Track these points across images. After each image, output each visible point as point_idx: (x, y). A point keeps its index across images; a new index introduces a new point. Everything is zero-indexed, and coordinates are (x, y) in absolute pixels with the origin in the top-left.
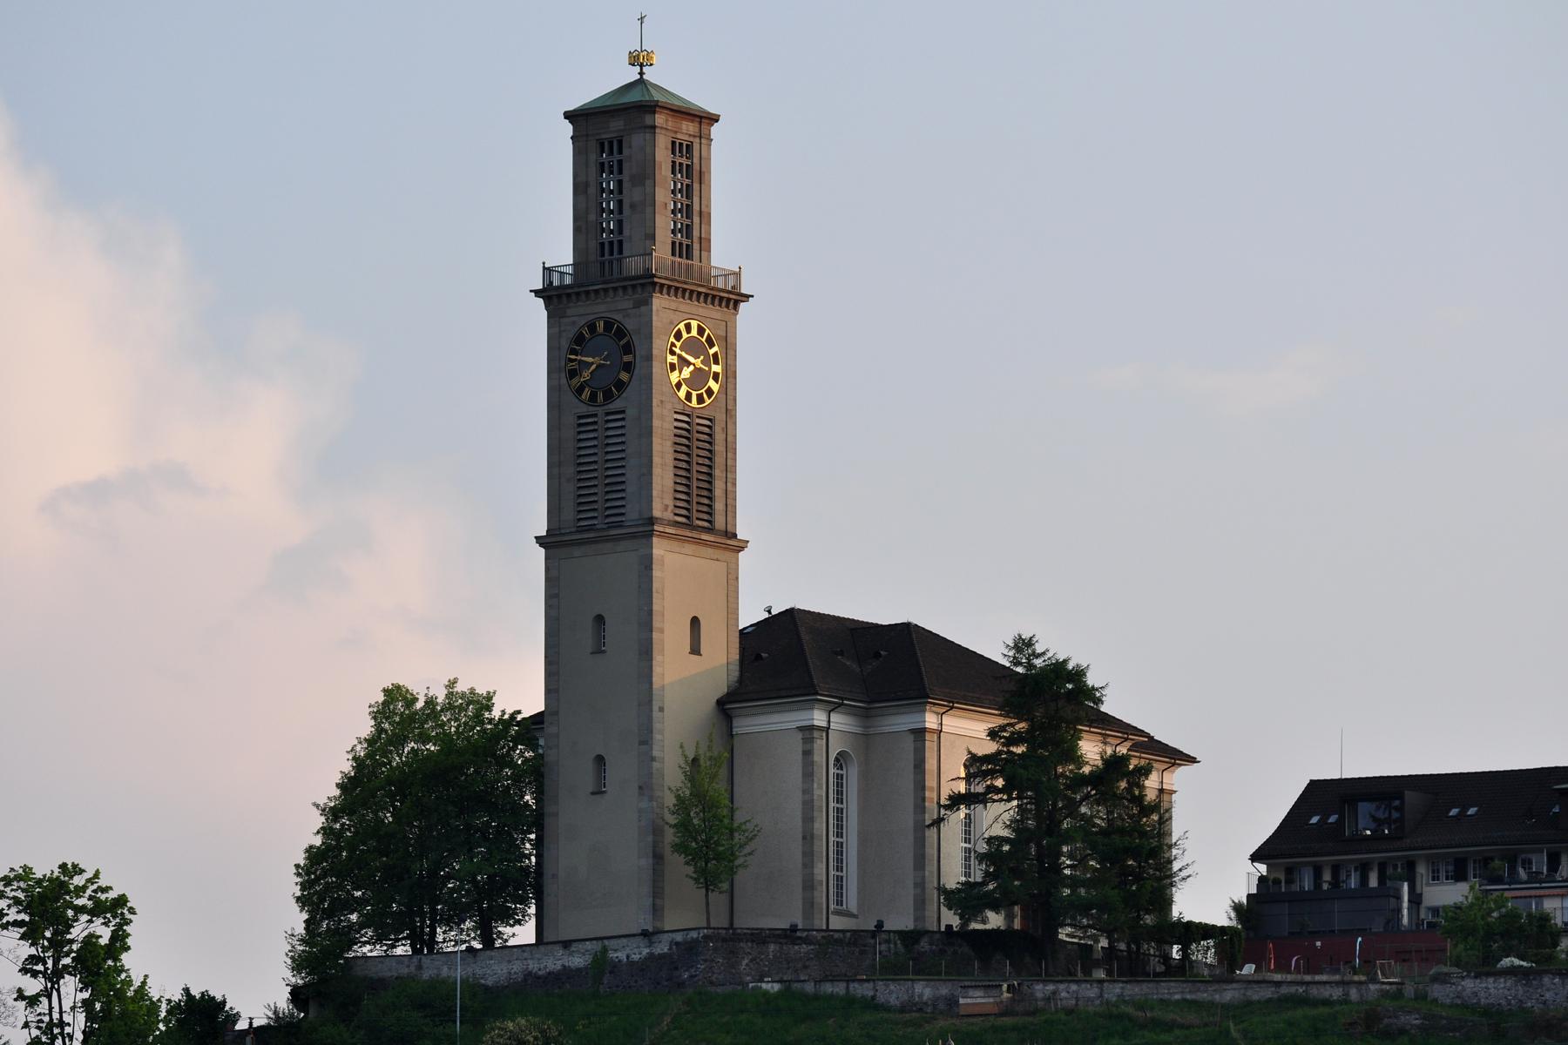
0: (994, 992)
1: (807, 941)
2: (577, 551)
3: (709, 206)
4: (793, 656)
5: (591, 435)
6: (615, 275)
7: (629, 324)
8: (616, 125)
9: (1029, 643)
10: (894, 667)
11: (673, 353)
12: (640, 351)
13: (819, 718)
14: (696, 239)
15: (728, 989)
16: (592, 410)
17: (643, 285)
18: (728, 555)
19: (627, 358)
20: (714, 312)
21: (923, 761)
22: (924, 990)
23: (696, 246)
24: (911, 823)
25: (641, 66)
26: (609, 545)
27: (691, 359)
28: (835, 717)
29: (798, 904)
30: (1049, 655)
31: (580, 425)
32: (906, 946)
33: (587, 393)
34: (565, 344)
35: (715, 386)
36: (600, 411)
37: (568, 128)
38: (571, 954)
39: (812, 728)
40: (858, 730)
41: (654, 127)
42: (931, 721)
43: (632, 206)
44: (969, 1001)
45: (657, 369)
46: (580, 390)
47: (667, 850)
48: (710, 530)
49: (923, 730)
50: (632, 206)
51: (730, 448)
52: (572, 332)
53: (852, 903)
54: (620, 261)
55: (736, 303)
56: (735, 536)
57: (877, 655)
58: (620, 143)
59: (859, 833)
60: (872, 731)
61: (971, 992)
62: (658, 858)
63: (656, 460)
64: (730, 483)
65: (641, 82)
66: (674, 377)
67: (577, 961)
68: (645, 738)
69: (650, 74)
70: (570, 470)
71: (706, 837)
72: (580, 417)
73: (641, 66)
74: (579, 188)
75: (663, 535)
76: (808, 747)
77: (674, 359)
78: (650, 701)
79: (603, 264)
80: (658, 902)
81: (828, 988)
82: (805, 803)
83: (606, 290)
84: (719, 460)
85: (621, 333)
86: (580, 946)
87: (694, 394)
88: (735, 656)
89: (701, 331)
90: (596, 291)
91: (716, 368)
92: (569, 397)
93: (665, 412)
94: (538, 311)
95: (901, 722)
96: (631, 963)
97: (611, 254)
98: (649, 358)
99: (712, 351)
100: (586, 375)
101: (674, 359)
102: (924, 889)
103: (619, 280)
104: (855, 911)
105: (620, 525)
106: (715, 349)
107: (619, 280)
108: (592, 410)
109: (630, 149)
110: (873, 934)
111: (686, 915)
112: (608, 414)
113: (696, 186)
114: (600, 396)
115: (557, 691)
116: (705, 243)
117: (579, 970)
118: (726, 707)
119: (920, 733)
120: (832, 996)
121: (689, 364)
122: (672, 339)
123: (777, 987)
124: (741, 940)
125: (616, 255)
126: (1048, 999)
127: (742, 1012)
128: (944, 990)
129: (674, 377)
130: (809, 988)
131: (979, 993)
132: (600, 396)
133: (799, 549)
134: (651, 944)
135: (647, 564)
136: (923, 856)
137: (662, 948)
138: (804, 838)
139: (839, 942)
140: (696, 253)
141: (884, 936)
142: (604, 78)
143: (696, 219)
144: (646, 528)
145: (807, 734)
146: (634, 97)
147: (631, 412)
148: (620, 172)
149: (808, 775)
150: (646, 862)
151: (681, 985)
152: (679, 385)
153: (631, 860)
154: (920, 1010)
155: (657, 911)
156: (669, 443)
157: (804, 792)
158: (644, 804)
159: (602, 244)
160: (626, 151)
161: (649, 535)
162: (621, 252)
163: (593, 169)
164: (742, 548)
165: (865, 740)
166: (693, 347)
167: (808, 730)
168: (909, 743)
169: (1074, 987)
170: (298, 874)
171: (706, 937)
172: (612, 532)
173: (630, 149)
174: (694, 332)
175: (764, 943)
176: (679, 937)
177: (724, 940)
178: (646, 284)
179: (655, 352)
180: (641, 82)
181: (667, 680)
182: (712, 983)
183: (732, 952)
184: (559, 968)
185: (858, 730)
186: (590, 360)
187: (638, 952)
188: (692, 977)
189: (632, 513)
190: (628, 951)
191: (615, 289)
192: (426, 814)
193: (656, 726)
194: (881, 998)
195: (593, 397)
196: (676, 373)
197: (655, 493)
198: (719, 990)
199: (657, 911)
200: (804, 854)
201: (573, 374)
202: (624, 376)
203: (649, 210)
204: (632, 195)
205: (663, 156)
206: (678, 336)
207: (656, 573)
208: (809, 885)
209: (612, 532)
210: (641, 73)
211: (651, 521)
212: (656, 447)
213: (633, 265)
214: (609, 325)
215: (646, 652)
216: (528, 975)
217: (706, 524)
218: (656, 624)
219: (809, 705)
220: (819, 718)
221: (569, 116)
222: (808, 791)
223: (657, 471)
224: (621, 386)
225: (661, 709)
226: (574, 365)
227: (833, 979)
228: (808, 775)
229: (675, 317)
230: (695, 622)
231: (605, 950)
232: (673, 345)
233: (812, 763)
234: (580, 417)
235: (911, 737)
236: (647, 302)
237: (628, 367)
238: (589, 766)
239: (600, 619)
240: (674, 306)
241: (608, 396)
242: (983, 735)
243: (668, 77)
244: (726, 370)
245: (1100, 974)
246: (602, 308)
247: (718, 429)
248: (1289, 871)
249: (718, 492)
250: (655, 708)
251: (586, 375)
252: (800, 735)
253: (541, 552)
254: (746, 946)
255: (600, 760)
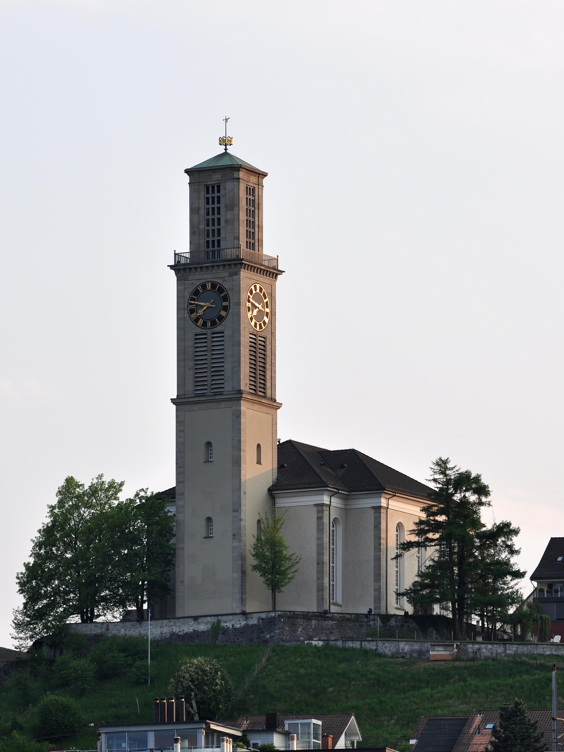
0: (449, 648)
1: (332, 619)
2: (195, 407)
3: (262, 222)
4: (301, 466)
5: (203, 345)
6: (211, 259)
7: (226, 285)
8: (216, 178)
9: (445, 462)
10: (358, 475)
11: (249, 301)
12: (233, 299)
13: (326, 499)
14: (256, 240)
15: (294, 644)
16: (204, 331)
17: (235, 264)
18: (272, 411)
19: (225, 304)
20: (266, 280)
21: (380, 523)
22: (405, 647)
23: (257, 244)
24: (372, 558)
25: (226, 145)
26: (215, 404)
27: (257, 305)
28: (333, 499)
29: (315, 599)
30: (456, 468)
31: (196, 339)
32: (383, 623)
33: (201, 322)
34: (187, 295)
35: (266, 320)
36: (209, 332)
37: (187, 178)
38: (199, 623)
39: (323, 505)
40: (342, 506)
41: (239, 179)
42: (383, 502)
43: (226, 221)
44: (435, 653)
45: (243, 310)
46: (196, 320)
47: (249, 569)
48: (265, 397)
49: (380, 507)
50: (226, 221)
51: (273, 353)
52: (191, 289)
53: (339, 599)
54: (219, 251)
55: (277, 275)
56: (275, 400)
57: (342, 467)
58: (219, 187)
59: (343, 561)
60: (349, 507)
61: (436, 648)
62: (243, 572)
63: (242, 359)
64: (273, 372)
65: (226, 154)
66: (249, 315)
67: (202, 627)
68: (237, 509)
69: (230, 150)
70: (191, 363)
71: (272, 564)
72: (196, 335)
73: (226, 145)
74: (193, 211)
75: (247, 400)
76: (320, 515)
77: (249, 305)
78: (240, 488)
79: (208, 252)
80: (244, 596)
81: (350, 644)
82: (318, 545)
83: (213, 267)
84: (268, 360)
85: (221, 290)
86: (204, 619)
87: (258, 323)
88: (276, 466)
89: (261, 290)
90: (207, 267)
91: (268, 310)
92: (190, 324)
93: (246, 333)
94: (172, 276)
95: (367, 503)
96: (235, 629)
97: (213, 246)
98: (238, 304)
99: (265, 301)
100: (201, 312)
101: (249, 305)
102: (380, 592)
103: (221, 261)
104: (340, 603)
105: (221, 394)
106: (267, 299)
107: (221, 261)
108: (204, 331)
109: (221, 192)
110: (366, 616)
111: (258, 605)
112: (213, 333)
113: (256, 211)
114: (209, 324)
115: (183, 482)
116: (260, 241)
117: (203, 632)
118: (273, 492)
119: (378, 509)
120: (353, 649)
121: (256, 307)
122: (249, 294)
123: (321, 643)
124: (297, 618)
125: (216, 248)
126: (475, 653)
127: (307, 656)
128: (416, 647)
129: (249, 315)
130: (339, 644)
131: (442, 649)
132: (209, 324)
133: (310, 407)
134: (247, 619)
135: (238, 415)
136: (380, 574)
137: (253, 621)
138: (318, 564)
139: (349, 620)
140: (256, 247)
141: (372, 617)
142: (206, 152)
143: (257, 229)
144: (238, 395)
145: (320, 508)
146: (225, 162)
147: (227, 333)
148: (219, 202)
149: (320, 530)
150: (237, 575)
151: (266, 641)
152: (251, 319)
153: (227, 573)
154: (403, 657)
155: (243, 601)
156: (248, 350)
157: (318, 539)
158: (236, 544)
159: (208, 242)
160: (222, 192)
161: (240, 399)
162: (219, 246)
163: (203, 202)
164: (279, 408)
165: (346, 511)
166: (257, 298)
167: (320, 507)
168: (371, 514)
169: (490, 646)
170: (18, 578)
171: (279, 616)
172: (217, 397)
173: (221, 192)
174: (258, 291)
175: (309, 620)
176: (263, 616)
177: (289, 618)
178: (237, 263)
179: (242, 301)
180: (226, 154)
181: (247, 478)
182: (283, 640)
183: (293, 624)
184: (191, 630)
185: (342, 506)
186: (203, 304)
187: (240, 623)
188: (271, 637)
189: (228, 387)
190: (233, 622)
191: (218, 266)
192: (99, 548)
193: (243, 502)
194: (381, 651)
195: (204, 325)
196: (251, 312)
197: (242, 377)
198: (288, 644)
199: (243, 601)
200: (318, 572)
201: (192, 311)
202: (223, 313)
203: (236, 223)
204: (225, 215)
205: (243, 194)
206: (251, 292)
207: (243, 420)
208: (320, 589)
209: (217, 397)
210: (226, 149)
211: (240, 392)
212: (242, 352)
213: (229, 253)
214: (214, 285)
215: (237, 462)
216: (173, 634)
217: (262, 394)
218: (242, 447)
219: (321, 493)
220: (326, 499)
221: (187, 171)
222: (320, 539)
223: (242, 365)
224: (221, 318)
225: (245, 493)
226: (193, 307)
227: (352, 639)
228: (320, 530)
229: (251, 282)
230: (259, 446)
231: (219, 622)
232: (249, 297)
233: (323, 524)
234: (196, 335)
235: (373, 511)
236: (237, 274)
237: (226, 309)
238: (203, 523)
239: (209, 444)
240: (249, 276)
241: (214, 324)
242: (419, 511)
243: (240, 152)
244: (271, 311)
245: (480, 639)
246: (211, 276)
247: (268, 343)
248: (550, 586)
249: (268, 377)
250: (242, 493)
251: (201, 312)
252: (315, 509)
253: (175, 406)
254: (300, 621)
255: (209, 520)
